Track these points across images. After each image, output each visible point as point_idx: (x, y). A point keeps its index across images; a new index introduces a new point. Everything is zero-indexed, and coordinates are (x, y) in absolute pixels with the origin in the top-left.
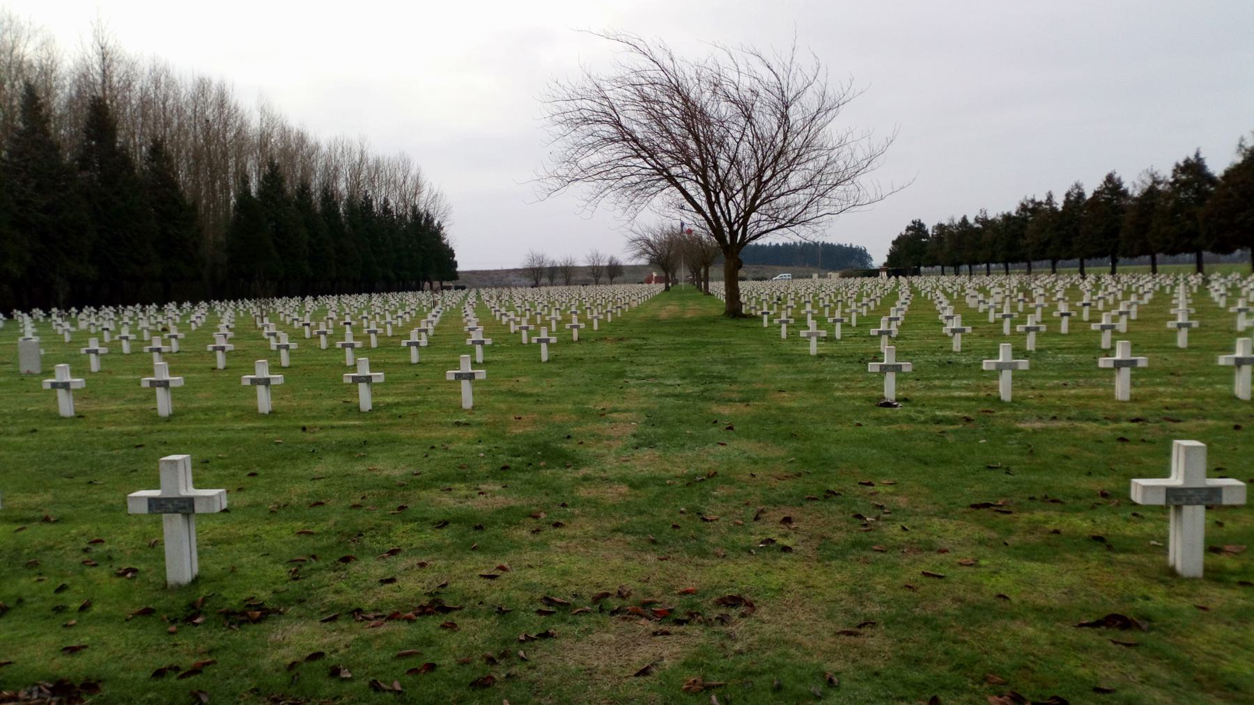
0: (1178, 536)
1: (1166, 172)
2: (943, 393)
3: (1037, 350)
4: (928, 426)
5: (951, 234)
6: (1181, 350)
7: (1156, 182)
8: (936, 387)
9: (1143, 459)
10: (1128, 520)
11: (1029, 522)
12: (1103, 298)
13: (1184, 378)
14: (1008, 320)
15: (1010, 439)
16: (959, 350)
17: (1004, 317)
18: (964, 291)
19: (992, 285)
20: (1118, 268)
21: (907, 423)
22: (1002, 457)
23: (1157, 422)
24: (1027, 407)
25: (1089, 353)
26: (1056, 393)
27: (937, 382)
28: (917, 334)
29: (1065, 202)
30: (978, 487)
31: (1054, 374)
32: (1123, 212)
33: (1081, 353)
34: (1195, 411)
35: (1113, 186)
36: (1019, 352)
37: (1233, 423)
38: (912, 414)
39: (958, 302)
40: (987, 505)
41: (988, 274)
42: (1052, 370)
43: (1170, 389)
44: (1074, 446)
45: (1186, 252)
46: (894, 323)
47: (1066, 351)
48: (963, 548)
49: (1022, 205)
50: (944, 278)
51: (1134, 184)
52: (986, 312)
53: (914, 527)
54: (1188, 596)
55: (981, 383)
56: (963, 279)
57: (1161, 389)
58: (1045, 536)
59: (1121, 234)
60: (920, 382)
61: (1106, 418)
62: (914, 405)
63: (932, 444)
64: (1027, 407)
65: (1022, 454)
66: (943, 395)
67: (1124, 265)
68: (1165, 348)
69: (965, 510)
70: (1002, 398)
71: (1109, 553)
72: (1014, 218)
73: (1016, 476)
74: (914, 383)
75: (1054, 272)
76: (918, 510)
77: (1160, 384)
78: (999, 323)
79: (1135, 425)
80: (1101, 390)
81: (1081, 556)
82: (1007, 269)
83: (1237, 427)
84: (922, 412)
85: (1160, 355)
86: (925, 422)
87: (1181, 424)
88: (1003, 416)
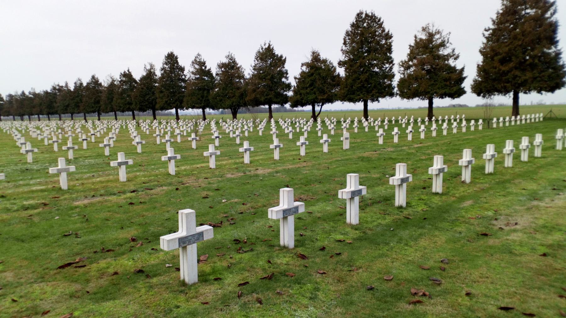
0: (185, 261)
1: (117, 77)
2: (26, 189)
3: (74, 158)
4: (20, 212)
5: (17, 100)
6: (140, 154)
7: (113, 81)
8: (20, 186)
9: (144, 213)
10: (150, 254)
11: (98, 271)
12: (99, 131)
13: (145, 167)
14: (56, 144)
15: (73, 213)
16: (31, 161)
17: (54, 142)
18: (28, 129)
19: (43, 126)
20: (101, 117)
21: (5, 213)
22: (71, 226)
23: (143, 191)
24: (77, 192)
25: (100, 158)
26: (90, 181)
27: (21, 182)
28: (4, 154)
29: (75, 87)
30: (61, 252)
31: (87, 171)
32: (101, 93)
33: (96, 158)
34: (156, 183)
35: (95, 81)
36: (69, 162)
37: (175, 187)
38: (8, 206)
39: (26, 135)
40: (69, 264)
41: (39, 120)
42: (84, 169)
43: (142, 173)
44: (109, 211)
45: (128, 111)
46: (112, 140)
47: (89, 158)
48: (60, 304)
49: (53, 87)
50: (15, 122)
51: (105, 81)
52: (43, 140)
53: (21, 297)
54: (196, 297)
55: (48, 180)
56: (26, 123)
57: (138, 174)
58: (110, 278)
59: (101, 103)
60: (10, 184)
61: (119, 192)
62: (9, 200)
63: (24, 226)
64: (77, 192)
65: (82, 222)
66: (26, 190)
67: (104, 116)
68: (132, 153)
69: (55, 271)
70: (62, 188)
71: (147, 280)
72: (50, 93)
73: (82, 238)
74: (6, 185)
75: (72, 119)
76: (22, 280)
77: (136, 171)
78: (51, 145)
79: (133, 194)
80: (111, 177)
81: (135, 287)
82: (39, 118)
83: (177, 189)
84: (15, 204)
85: (131, 157)
86: (18, 210)
87: (153, 190)
88: (65, 199)
